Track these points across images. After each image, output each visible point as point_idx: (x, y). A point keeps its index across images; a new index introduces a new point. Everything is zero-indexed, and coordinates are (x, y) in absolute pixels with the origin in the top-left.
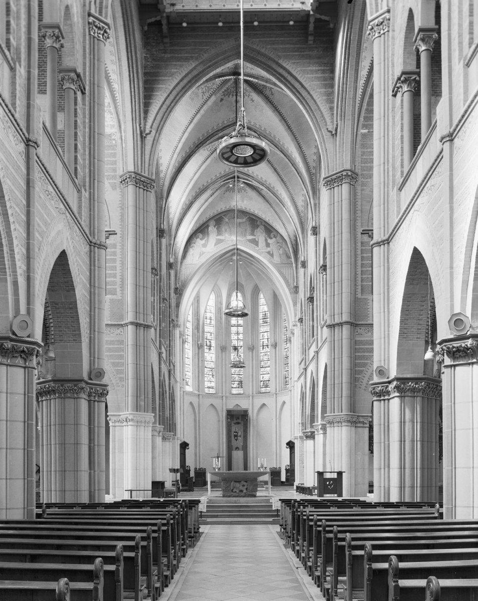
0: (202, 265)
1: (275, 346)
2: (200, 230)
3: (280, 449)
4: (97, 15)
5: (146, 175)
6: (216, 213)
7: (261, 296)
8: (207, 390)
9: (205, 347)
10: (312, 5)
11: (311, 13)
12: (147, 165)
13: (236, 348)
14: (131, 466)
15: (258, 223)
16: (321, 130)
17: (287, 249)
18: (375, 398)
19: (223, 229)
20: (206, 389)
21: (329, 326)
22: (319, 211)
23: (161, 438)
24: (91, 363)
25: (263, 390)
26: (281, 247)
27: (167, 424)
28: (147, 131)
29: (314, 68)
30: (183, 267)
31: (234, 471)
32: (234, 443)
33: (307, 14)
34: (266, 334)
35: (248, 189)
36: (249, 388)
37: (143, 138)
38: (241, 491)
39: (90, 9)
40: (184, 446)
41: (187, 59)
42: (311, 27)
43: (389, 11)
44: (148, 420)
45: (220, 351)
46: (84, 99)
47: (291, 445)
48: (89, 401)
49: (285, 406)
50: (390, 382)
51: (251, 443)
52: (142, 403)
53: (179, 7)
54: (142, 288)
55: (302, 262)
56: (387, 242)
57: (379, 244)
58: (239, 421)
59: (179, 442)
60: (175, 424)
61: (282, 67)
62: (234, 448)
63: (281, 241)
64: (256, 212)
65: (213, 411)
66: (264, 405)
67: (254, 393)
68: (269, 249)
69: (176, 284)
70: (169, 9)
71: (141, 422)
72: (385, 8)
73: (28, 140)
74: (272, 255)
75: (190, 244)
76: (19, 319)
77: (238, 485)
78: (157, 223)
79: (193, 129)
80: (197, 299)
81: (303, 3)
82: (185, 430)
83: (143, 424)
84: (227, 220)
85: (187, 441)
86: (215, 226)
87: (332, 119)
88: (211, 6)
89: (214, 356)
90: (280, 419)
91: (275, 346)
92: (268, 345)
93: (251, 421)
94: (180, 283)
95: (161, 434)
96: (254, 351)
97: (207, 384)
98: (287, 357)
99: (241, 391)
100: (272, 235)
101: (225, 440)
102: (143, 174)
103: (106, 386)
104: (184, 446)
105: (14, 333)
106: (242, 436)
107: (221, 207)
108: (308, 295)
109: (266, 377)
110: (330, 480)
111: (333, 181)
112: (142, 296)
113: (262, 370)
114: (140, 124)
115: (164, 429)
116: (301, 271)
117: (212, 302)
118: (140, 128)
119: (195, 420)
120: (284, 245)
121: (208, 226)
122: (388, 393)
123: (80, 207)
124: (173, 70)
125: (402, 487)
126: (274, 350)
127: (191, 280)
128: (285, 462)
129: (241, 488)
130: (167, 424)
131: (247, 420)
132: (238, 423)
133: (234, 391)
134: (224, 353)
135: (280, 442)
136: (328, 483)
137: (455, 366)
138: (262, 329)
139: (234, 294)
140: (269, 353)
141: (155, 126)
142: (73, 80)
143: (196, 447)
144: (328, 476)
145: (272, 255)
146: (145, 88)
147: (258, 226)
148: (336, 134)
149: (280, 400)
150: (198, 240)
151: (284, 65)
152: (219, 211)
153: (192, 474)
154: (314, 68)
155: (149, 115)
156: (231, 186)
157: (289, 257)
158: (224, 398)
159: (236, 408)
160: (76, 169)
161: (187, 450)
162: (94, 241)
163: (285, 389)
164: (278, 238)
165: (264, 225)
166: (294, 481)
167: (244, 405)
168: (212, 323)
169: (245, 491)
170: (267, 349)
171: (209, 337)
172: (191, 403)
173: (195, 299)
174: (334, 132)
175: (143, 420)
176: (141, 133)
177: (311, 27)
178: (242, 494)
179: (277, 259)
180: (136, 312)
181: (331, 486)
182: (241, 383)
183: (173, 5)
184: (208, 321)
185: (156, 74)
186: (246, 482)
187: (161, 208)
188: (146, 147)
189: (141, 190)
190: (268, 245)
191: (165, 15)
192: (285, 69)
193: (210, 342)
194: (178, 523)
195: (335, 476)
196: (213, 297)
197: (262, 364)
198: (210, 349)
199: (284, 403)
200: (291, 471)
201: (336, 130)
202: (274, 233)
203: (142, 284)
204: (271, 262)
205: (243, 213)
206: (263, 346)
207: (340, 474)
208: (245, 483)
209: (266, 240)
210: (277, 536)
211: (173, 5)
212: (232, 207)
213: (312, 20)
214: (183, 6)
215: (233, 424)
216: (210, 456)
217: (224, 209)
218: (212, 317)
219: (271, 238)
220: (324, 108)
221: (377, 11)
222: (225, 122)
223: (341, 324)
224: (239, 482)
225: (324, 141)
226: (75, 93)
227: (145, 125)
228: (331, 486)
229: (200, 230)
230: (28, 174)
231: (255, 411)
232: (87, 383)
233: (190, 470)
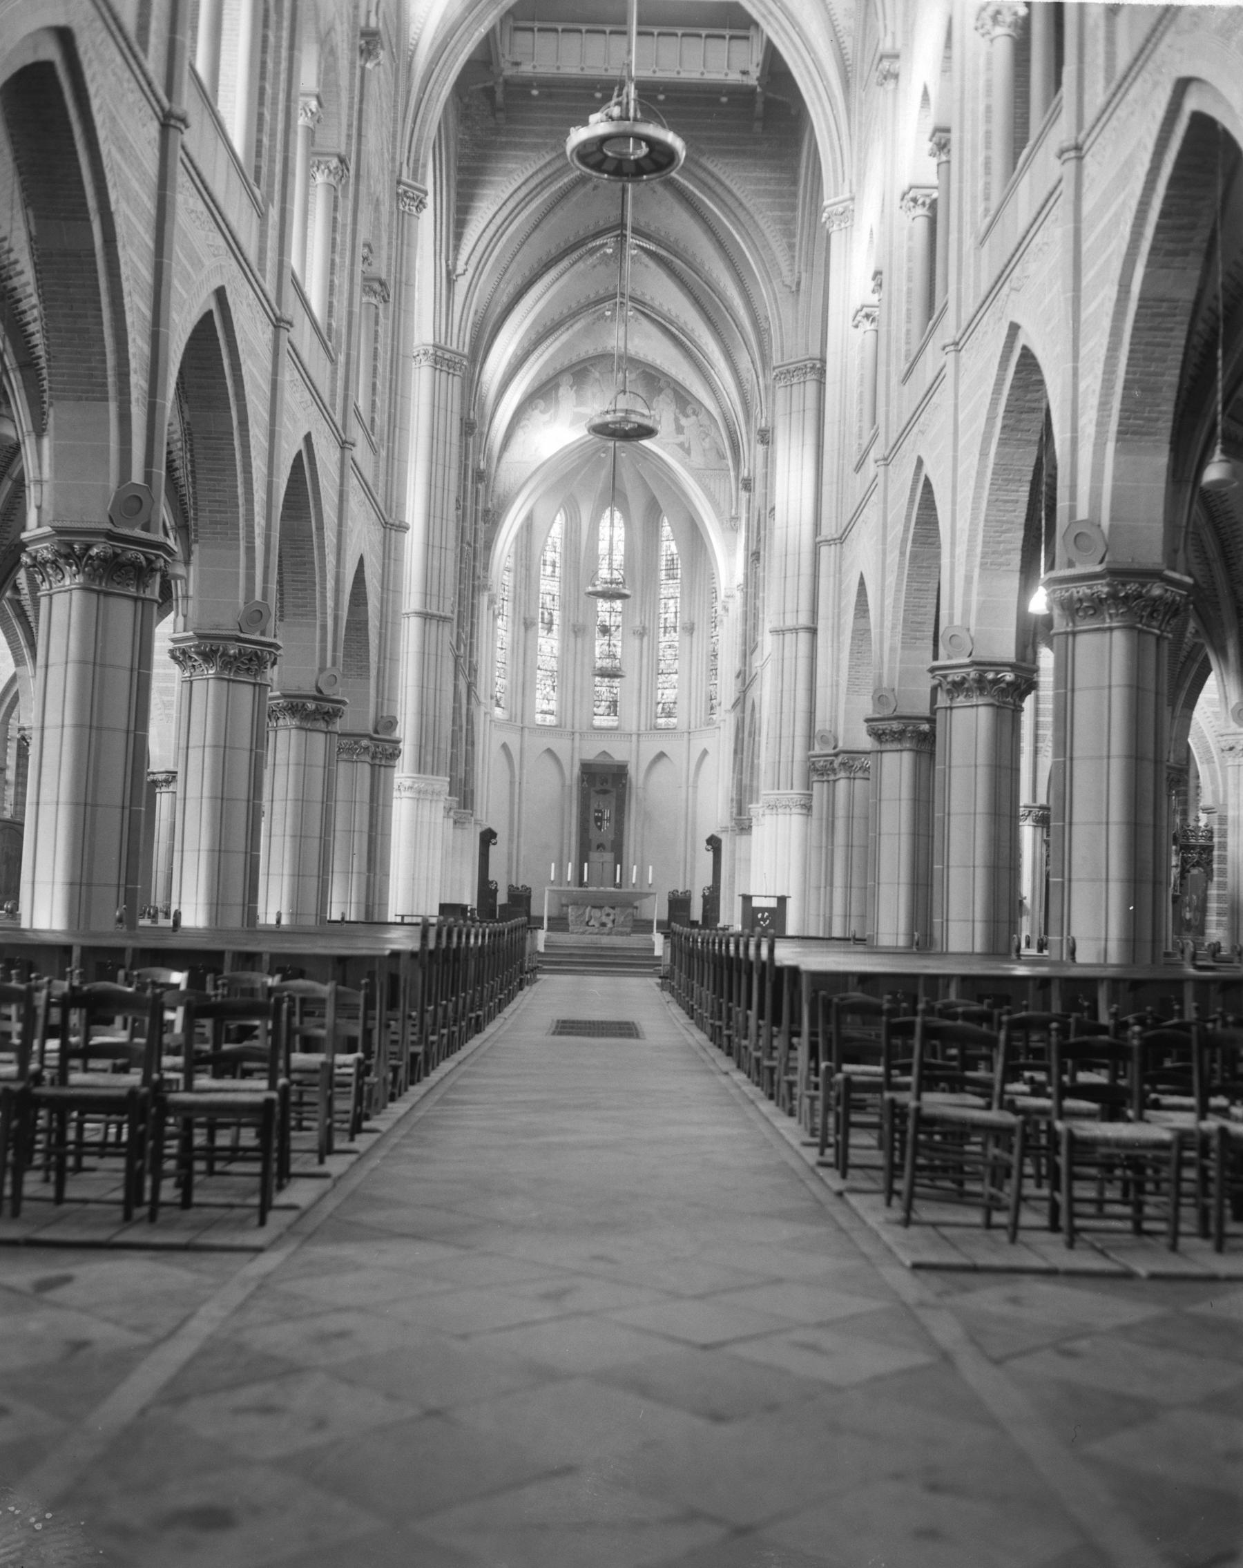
0: (543, 464)
1: (690, 629)
2: (543, 392)
3: (694, 850)
4: (410, 182)
5: (454, 347)
6: (575, 359)
7: (666, 522)
8: (539, 718)
9: (540, 625)
10: (758, 79)
11: (759, 90)
12: (455, 331)
13: (605, 630)
14: (419, 874)
15: (662, 384)
16: (771, 282)
17: (718, 440)
18: (815, 778)
19: (589, 394)
20: (539, 717)
21: (775, 632)
22: (774, 400)
23: (451, 821)
24: (379, 706)
25: (662, 721)
26: (707, 435)
27: (463, 795)
28: (460, 270)
29: (763, 175)
30: (503, 465)
31: (620, 184)
32: (594, 834)
33: (751, 91)
34: (671, 602)
35: (641, 317)
36: (630, 717)
37: (451, 282)
38: (603, 925)
39: (400, 175)
40: (488, 837)
41: (535, 147)
42: (759, 107)
43: (852, 199)
44: (437, 787)
45: (572, 639)
46: (386, 309)
47: (714, 843)
48: (372, 766)
49: (708, 759)
50: (836, 755)
51: (632, 838)
52: (429, 759)
53: (527, 69)
54: (437, 550)
55: (744, 479)
56: (841, 540)
57: (828, 542)
58: (608, 787)
59: (479, 830)
60: (472, 791)
61: (705, 169)
62: (594, 846)
63: (707, 422)
64: (658, 362)
65: (548, 762)
66: (662, 755)
67: (643, 728)
68: (681, 438)
69: (486, 502)
70: (509, 72)
71: (426, 792)
72: (847, 195)
73: (344, 442)
74: (688, 451)
75: (518, 422)
76: (326, 674)
77: (596, 913)
78: (393, 159)
79: (550, 302)
80: (528, 525)
81: (744, 73)
82: (491, 806)
83: (429, 797)
84: (597, 375)
85: (494, 828)
86: (571, 387)
87: (792, 264)
88: (582, 69)
89: (556, 644)
90: (695, 787)
91: (690, 629)
92: (675, 628)
93: (634, 791)
94: (495, 501)
95: (452, 814)
96: (646, 639)
97: (541, 704)
98: (715, 656)
99: (609, 721)
100: (689, 411)
101: (574, 822)
102: (449, 346)
103: (398, 742)
104: (488, 837)
105: (320, 691)
106: (613, 820)
107: (588, 348)
108: (753, 547)
109: (670, 695)
110: (763, 910)
111: (788, 373)
112: (436, 563)
113: (662, 678)
114: (447, 260)
115: (459, 802)
116: (744, 495)
117: (557, 530)
118: (447, 266)
119: (512, 783)
120: (713, 432)
121: (557, 386)
122: (834, 770)
123: (376, 476)
124: (510, 166)
125: (847, 916)
126: (688, 639)
127: (517, 494)
128: (704, 879)
129: (604, 919)
130: (463, 795)
131: (624, 785)
132: (605, 792)
133: (598, 721)
134: (579, 640)
135: (694, 838)
136: (760, 916)
137: (882, 752)
138: (664, 592)
139: (608, 512)
140: (676, 644)
141: (474, 260)
142: (375, 293)
143: (511, 840)
144: (756, 903)
145: (688, 451)
146: (458, 194)
147: (661, 390)
148: (798, 290)
149: (698, 744)
150: (536, 412)
151: (710, 166)
152: (583, 355)
153: (502, 898)
154: (763, 175)
155: (464, 241)
156: (608, 313)
157: (722, 457)
158: (577, 736)
159: (602, 760)
160: (373, 420)
161: (492, 848)
162: (391, 521)
163: (709, 723)
164: (703, 417)
165: (675, 391)
166: (717, 920)
167: (619, 752)
168: (557, 574)
169: (610, 925)
170: (675, 636)
171: (549, 605)
172: (505, 747)
173: (521, 527)
174: (794, 289)
175: (430, 788)
176: (449, 273)
177: (759, 107)
178: (606, 930)
179: (697, 459)
180: (426, 594)
181: (765, 921)
182: (613, 707)
183: (517, 64)
184: (549, 569)
185: (480, 171)
186: (613, 908)
187: (472, 381)
188: (456, 298)
189: (444, 375)
190: (680, 429)
191: (501, 80)
192: (713, 176)
193: (551, 614)
194: (464, 1015)
195: (772, 903)
196: (560, 520)
197: (662, 665)
198: (550, 630)
199: (705, 752)
200: (712, 900)
201: (799, 284)
202: (695, 406)
203: (437, 543)
204: (684, 465)
205: (633, 362)
206: (665, 627)
207: (782, 900)
208: (611, 911)
209: (677, 420)
210: (658, 989)
211: (517, 64)
212: (609, 348)
213: (760, 99)
214: (534, 67)
215: (593, 794)
216: (542, 865)
217: (591, 352)
218: (557, 560)
219: (687, 416)
220: (777, 245)
221: (836, 195)
222: (601, 223)
223: (795, 630)
224: (601, 907)
225: (776, 300)
226: (377, 307)
227: (456, 259)
228: (765, 921)
229: (543, 392)
230: (342, 484)
231: (644, 765)
232: (372, 739)
233: (496, 890)
